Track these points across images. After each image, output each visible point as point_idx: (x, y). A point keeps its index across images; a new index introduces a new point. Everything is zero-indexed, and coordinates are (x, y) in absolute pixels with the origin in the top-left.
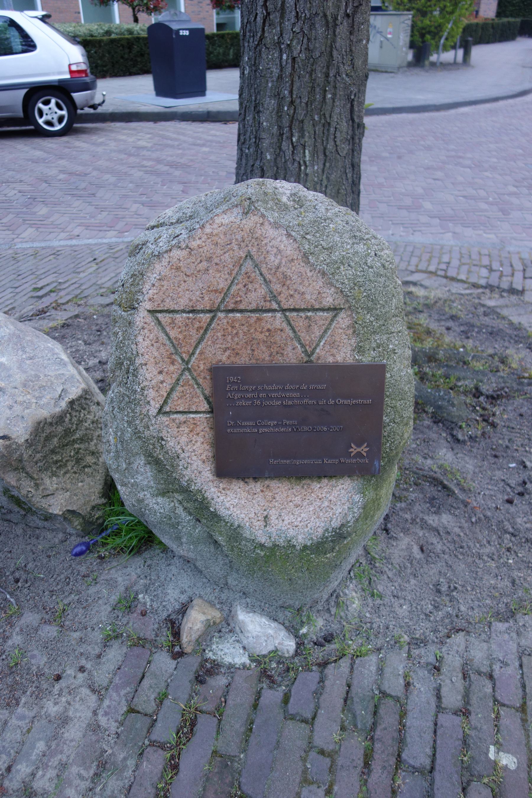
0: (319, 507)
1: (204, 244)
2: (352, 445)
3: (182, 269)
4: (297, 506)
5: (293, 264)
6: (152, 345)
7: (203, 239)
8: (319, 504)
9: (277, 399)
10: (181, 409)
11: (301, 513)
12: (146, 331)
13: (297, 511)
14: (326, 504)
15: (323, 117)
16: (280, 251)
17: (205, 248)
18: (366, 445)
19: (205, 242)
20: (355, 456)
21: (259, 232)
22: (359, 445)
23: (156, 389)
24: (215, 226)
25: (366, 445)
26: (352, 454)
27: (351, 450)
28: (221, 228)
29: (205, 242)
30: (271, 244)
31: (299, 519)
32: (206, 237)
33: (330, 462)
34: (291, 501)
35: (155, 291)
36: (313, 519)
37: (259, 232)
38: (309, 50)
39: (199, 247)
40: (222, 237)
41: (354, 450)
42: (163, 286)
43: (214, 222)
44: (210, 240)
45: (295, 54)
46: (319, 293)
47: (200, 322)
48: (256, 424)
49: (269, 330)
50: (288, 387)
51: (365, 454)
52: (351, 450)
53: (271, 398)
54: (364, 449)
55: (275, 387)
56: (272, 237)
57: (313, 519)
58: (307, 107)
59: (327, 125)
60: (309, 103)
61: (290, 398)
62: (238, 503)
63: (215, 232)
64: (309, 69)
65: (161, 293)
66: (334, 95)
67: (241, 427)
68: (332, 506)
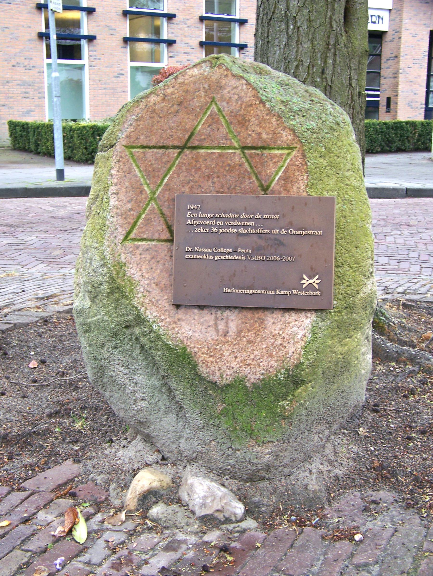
0: (272, 344)
1: (176, 91)
2: (305, 277)
3: (157, 111)
4: (249, 342)
5: (252, 108)
6: (125, 176)
7: (176, 87)
8: (272, 341)
9: (233, 226)
10: (145, 236)
11: (254, 350)
12: (121, 163)
13: (250, 348)
14: (279, 341)
15: (324, 80)
16: (240, 97)
17: (177, 94)
18: (317, 277)
19: (177, 90)
20: (306, 289)
21: (224, 82)
22: (310, 277)
23: (124, 216)
24: (187, 77)
25: (317, 277)
26: (304, 286)
27: (303, 281)
28: (191, 79)
29: (177, 90)
30: (233, 92)
31: (252, 357)
32: (178, 86)
33: (282, 292)
34: (244, 337)
35: (132, 130)
36: (265, 357)
37: (224, 82)
38: (310, 21)
39: (173, 93)
40: (192, 85)
41: (306, 281)
42: (139, 125)
43: (186, 74)
44: (181, 88)
45: (299, 24)
46: (274, 133)
47: (168, 157)
48: (213, 250)
49: (229, 165)
50: (243, 216)
51: (317, 286)
52: (303, 281)
53: (228, 227)
54: (315, 281)
55: (231, 215)
56: (234, 86)
57: (265, 357)
58: (309, 70)
59: (328, 88)
60: (311, 66)
61: (245, 227)
62: (193, 331)
63: (186, 82)
64: (311, 36)
65: (137, 131)
66: (334, 60)
67: (198, 253)
68: (285, 344)
